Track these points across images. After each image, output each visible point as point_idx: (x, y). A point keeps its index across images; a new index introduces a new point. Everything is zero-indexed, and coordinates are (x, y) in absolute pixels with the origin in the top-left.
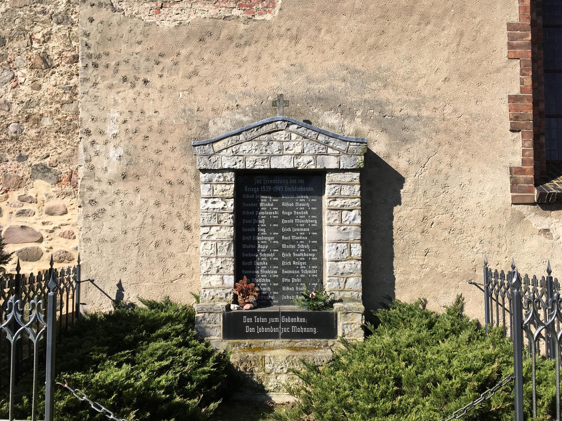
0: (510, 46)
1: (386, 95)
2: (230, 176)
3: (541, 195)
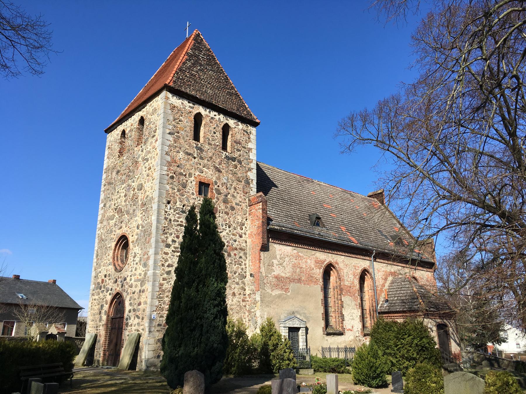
1: (306, 312)
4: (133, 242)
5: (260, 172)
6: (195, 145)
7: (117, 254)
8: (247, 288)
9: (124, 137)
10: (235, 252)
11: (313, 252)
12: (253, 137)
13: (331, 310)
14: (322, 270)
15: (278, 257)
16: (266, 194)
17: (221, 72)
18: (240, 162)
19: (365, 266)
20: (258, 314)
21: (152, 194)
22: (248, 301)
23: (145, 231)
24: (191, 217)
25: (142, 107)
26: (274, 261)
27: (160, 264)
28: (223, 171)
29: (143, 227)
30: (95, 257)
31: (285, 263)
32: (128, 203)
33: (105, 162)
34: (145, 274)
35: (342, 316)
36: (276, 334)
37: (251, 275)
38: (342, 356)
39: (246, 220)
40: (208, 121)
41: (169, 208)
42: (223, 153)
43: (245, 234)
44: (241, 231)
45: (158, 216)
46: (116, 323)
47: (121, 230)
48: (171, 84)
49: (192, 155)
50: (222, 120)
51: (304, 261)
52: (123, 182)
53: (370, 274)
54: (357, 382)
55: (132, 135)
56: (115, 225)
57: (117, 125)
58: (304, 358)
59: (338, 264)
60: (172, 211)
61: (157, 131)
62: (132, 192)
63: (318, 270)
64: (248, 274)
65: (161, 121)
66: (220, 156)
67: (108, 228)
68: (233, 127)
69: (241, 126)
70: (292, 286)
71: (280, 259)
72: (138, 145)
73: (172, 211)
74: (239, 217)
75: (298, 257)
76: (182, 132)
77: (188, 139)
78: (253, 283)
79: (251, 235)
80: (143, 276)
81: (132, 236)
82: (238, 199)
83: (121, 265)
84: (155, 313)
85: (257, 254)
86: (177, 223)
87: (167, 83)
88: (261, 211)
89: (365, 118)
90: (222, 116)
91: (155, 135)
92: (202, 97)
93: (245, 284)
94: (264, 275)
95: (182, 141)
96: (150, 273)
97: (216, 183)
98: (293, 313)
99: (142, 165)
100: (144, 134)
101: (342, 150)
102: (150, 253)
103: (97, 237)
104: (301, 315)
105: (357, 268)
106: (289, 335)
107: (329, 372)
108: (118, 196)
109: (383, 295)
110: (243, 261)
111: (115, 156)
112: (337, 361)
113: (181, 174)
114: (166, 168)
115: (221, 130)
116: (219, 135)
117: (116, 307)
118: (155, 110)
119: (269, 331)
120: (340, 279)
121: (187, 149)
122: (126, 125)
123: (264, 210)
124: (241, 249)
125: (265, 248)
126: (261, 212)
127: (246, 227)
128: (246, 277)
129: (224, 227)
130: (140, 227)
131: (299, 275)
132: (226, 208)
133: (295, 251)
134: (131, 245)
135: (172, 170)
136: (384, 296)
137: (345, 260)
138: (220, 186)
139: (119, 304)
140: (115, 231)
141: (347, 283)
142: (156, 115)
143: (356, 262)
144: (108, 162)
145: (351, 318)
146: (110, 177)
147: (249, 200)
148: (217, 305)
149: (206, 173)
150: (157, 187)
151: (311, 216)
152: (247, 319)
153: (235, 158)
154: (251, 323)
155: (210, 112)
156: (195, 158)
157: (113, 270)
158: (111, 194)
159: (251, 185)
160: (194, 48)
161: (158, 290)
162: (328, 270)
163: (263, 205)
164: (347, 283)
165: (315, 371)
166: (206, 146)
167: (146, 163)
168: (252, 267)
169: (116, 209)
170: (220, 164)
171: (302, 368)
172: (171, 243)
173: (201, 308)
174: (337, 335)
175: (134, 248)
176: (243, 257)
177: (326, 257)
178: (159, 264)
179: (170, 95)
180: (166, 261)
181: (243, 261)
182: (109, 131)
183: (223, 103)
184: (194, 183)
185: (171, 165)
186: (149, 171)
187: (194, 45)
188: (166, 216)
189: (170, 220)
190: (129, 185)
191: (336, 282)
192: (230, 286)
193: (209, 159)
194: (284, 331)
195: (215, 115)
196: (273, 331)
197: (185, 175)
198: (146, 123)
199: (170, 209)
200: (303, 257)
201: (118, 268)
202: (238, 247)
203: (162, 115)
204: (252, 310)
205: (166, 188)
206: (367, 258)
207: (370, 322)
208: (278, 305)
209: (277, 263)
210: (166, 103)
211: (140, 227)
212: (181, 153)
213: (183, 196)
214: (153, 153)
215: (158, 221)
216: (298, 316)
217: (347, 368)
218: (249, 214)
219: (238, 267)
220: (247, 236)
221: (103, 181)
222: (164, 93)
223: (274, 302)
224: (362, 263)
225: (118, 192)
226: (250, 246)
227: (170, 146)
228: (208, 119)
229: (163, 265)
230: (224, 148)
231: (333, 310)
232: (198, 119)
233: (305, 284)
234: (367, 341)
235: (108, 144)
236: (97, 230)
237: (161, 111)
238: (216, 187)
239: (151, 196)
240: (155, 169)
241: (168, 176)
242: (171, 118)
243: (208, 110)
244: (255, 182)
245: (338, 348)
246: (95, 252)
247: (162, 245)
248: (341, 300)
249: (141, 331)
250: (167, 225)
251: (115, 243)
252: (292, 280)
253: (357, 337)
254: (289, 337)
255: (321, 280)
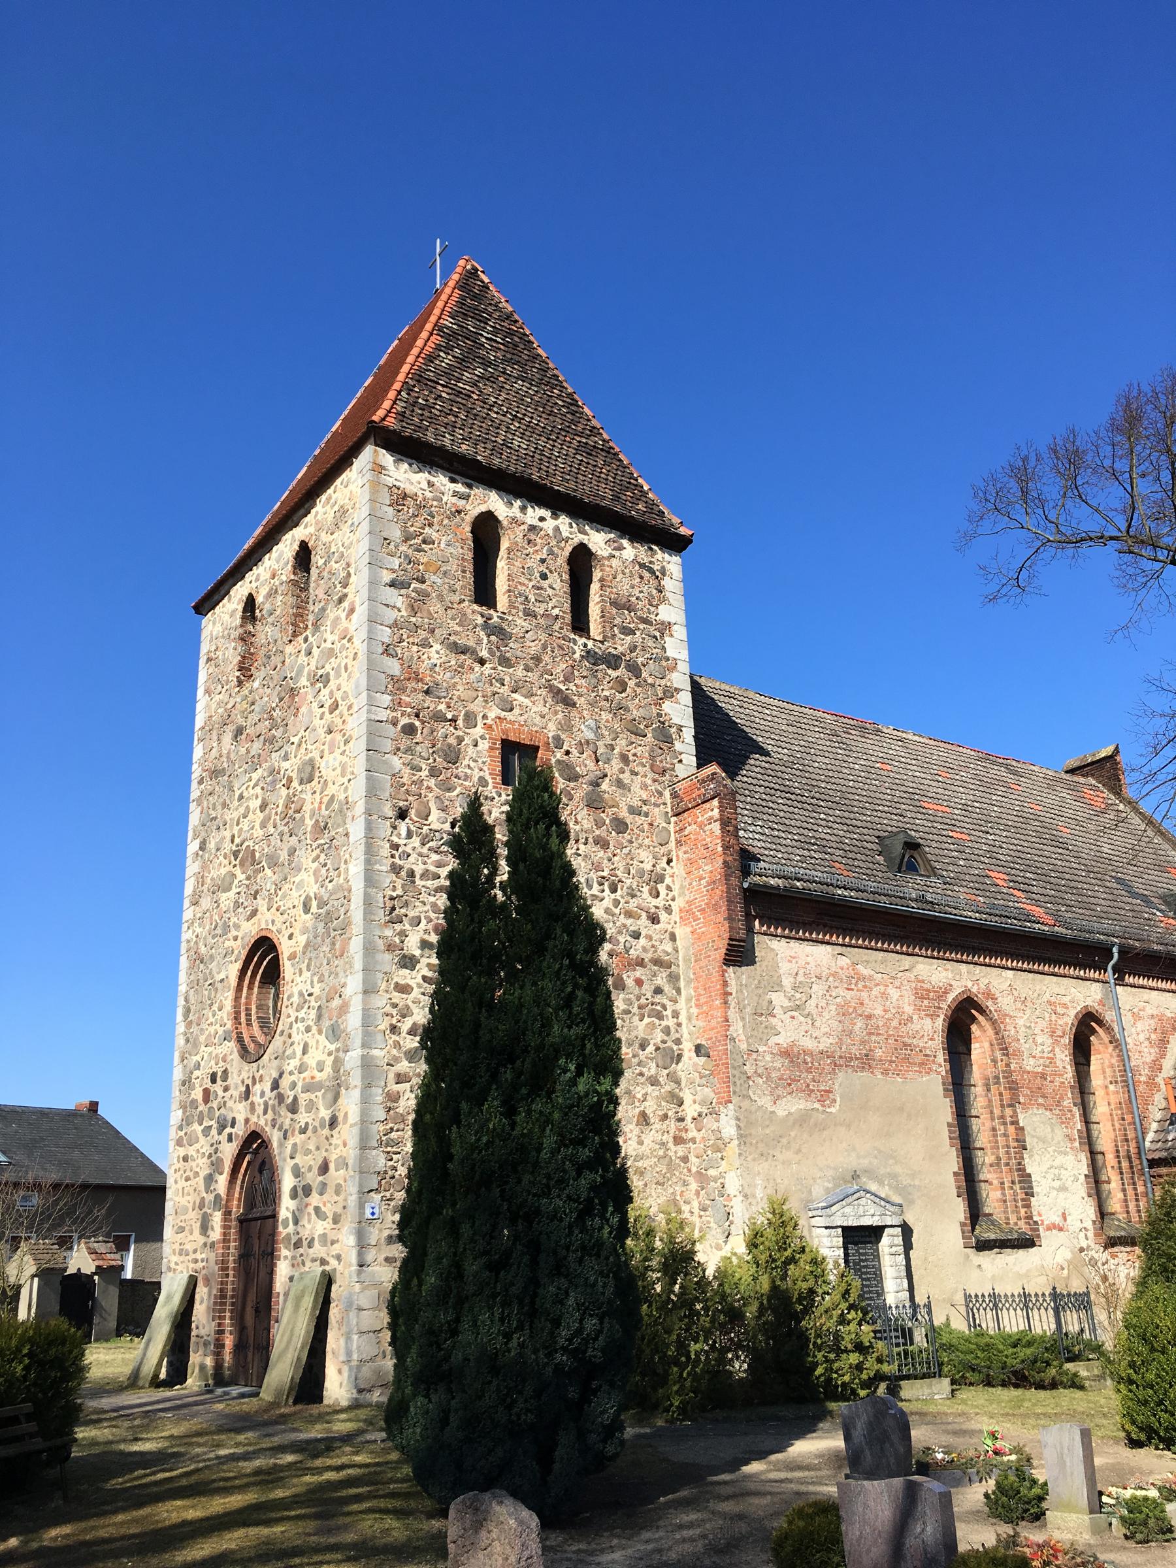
0: (950, 1138)
1: (898, 1169)
2: (840, 1230)
3: (978, 1241)
4: (292, 957)
5: (706, 709)
6: (480, 620)
7: (248, 1003)
8: (687, 1096)
9: (253, 619)
10: (639, 973)
11: (907, 961)
12: (672, 585)
13: (984, 1160)
14: (940, 1023)
15: (787, 982)
16: (732, 774)
17: (554, 382)
18: (634, 669)
19: (1089, 1002)
20: (733, 1184)
21: (346, 789)
22: (693, 1140)
23: (328, 918)
24: (471, 837)
25: (302, 511)
26: (773, 996)
27: (384, 1025)
28: (581, 702)
29: (322, 904)
30: (179, 1017)
31: (812, 1003)
32: (272, 830)
33: (199, 707)
34: (337, 1064)
35: (1025, 1178)
36: (806, 1257)
37: (698, 1049)
38: (1043, 1324)
39: (669, 861)
40: (519, 539)
41: (404, 833)
42: (575, 642)
43: (668, 910)
44: (655, 902)
45: (368, 862)
46: (254, 1233)
47: (255, 919)
48: (391, 423)
49: (474, 652)
50: (565, 534)
51: (876, 991)
52: (254, 762)
53: (1109, 1030)
54: (1143, 1437)
55: (277, 607)
56: (237, 905)
57: (231, 582)
58: (907, 1335)
59: (994, 999)
60: (416, 841)
61: (353, 579)
62: (284, 792)
63: (928, 1021)
64: (688, 1047)
65: (364, 546)
66: (568, 654)
67: (216, 917)
68: (605, 554)
69: (630, 551)
70: (842, 1081)
71: (795, 988)
72: (295, 635)
73: (416, 841)
74: (644, 854)
75: (854, 980)
76: (433, 578)
77: (456, 598)
78: (706, 1078)
79: (688, 914)
80: (328, 1070)
81: (290, 937)
82: (637, 794)
83: (261, 1039)
84: (377, 1197)
85: (716, 976)
86: (436, 883)
87: (375, 418)
88: (716, 827)
89: (1071, 461)
90: (564, 521)
91: (346, 595)
92: (496, 461)
93: (678, 1082)
94: (743, 1046)
95: (435, 607)
96: (353, 1058)
97: (559, 743)
98: (855, 1176)
99: (310, 698)
100: (312, 597)
101: (993, 587)
102: (348, 991)
103: (183, 950)
104: (881, 1183)
105: (1060, 1010)
106: (846, 1255)
107: (1004, 1384)
108: (242, 810)
109: (1159, 1100)
110: (668, 1004)
111: (228, 682)
112: (1029, 1344)
113: (439, 717)
114: (386, 699)
115: (566, 567)
116: (559, 584)
117: (251, 1184)
118: (343, 513)
119: (777, 1243)
120: (1005, 1049)
121: (456, 633)
122: (257, 580)
123: (729, 825)
124: (657, 962)
125: (739, 954)
126: (718, 832)
127: (669, 888)
128: (680, 1056)
129: (596, 890)
130: (314, 904)
131: (863, 1042)
132: (599, 824)
133: (844, 961)
134: (288, 969)
135: (408, 705)
136: (1163, 1104)
137: (1018, 984)
138: (574, 752)
139: (261, 1172)
140: (237, 927)
141: (1032, 1061)
142: (346, 528)
143: (1057, 990)
144: (208, 706)
145: (1057, 1184)
146: (214, 753)
147: (675, 795)
148: (589, 1165)
149: (525, 709)
150: (359, 766)
151: (887, 842)
152: (695, 1204)
153: (618, 658)
154: (710, 1218)
155: (523, 509)
156: (482, 662)
157: (236, 1056)
158: (219, 807)
159: (678, 746)
160: (462, 311)
161: (382, 1115)
162: (962, 1020)
163: (722, 807)
164: (1030, 1064)
165: (953, 1382)
166: (519, 622)
167: (323, 691)
168: (700, 1023)
169: (236, 854)
170: (567, 679)
171: (908, 1377)
172: (417, 953)
173: (527, 1178)
174: (1013, 1247)
175: (298, 979)
176: (667, 988)
177: (954, 976)
178: (382, 1027)
179: (387, 458)
180: (404, 1016)
181: (668, 1004)
182: (207, 606)
183: (564, 480)
184: (484, 745)
185: (404, 690)
186: (332, 716)
187: (461, 303)
188: (397, 860)
189: (411, 874)
190: (273, 772)
191: (994, 1061)
192: (628, 1092)
193: (531, 663)
194: (826, 1242)
195: (542, 519)
196: (796, 1243)
197: (454, 720)
198: (317, 560)
199: (409, 835)
200: (871, 978)
201: (251, 1047)
202: (647, 957)
203: (365, 527)
204: (712, 1172)
205: (391, 767)
206: (1091, 974)
207: (1120, 1195)
208: (799, 1151)
209: (786, 1003)
210: (375, 485)
211: (314, 904)
212: (437, 647)
213: (449, 790)
214: (344, 654)
215: (370, 880)
216: (873, 1187)
217: (1068, 1366)
218: (679, 843)
219: (652, 1026)
220: (676, 916)
221: (195, 767)
222: (369, 453)
223: (784, 1141)
224: (1078, 992)
225: (241, 797)
226: (687, 949)
227: (395, 625)
228: (520, 531)
229: (394, 1029)
230: (580, 624)
231: (990, 1159)
232: (486, 532)
233: (885, 1073)
234: (1125, 1268)
235: (205, 648)
236: (185, 926)
237: (360, 514)
238: (559, 755)
239: (342, 797)
240: (350, 708)
241: (395, 724)
242: (396, 534)
243: (518, 503)
244: (689, 734)
245: (1026, 1296)
246: (181, 1001)
247: (387, 960)
248: (1015, 1123)
249: (333, 1263)
250: (399, 892)
251: (239, 965)
252: (839, 1061)
253: (1082, 1250)
254: (847, 1262)
255: (941, 1057)
